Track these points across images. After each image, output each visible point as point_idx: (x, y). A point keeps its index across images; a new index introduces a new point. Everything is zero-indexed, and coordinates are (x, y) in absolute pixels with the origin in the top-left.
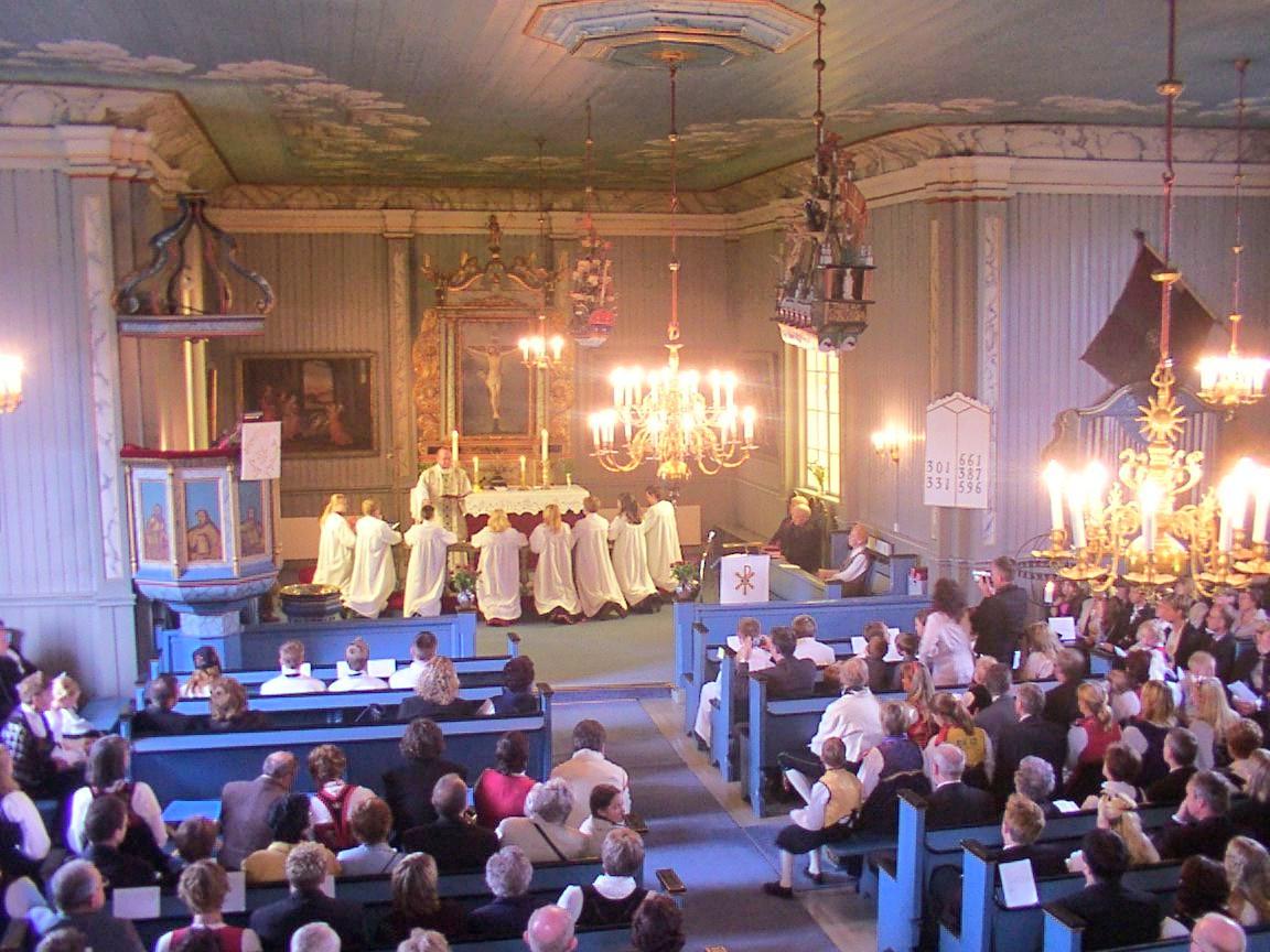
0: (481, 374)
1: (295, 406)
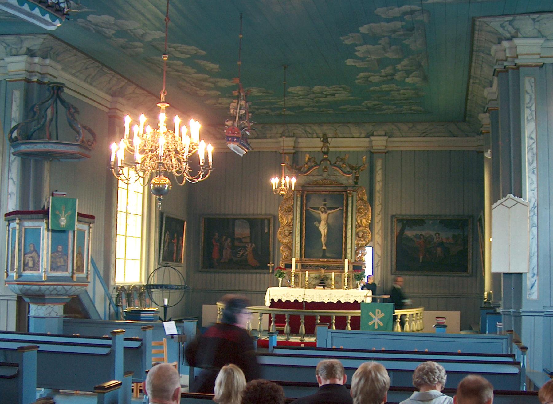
0: (316, 223)
1: (229, 244)
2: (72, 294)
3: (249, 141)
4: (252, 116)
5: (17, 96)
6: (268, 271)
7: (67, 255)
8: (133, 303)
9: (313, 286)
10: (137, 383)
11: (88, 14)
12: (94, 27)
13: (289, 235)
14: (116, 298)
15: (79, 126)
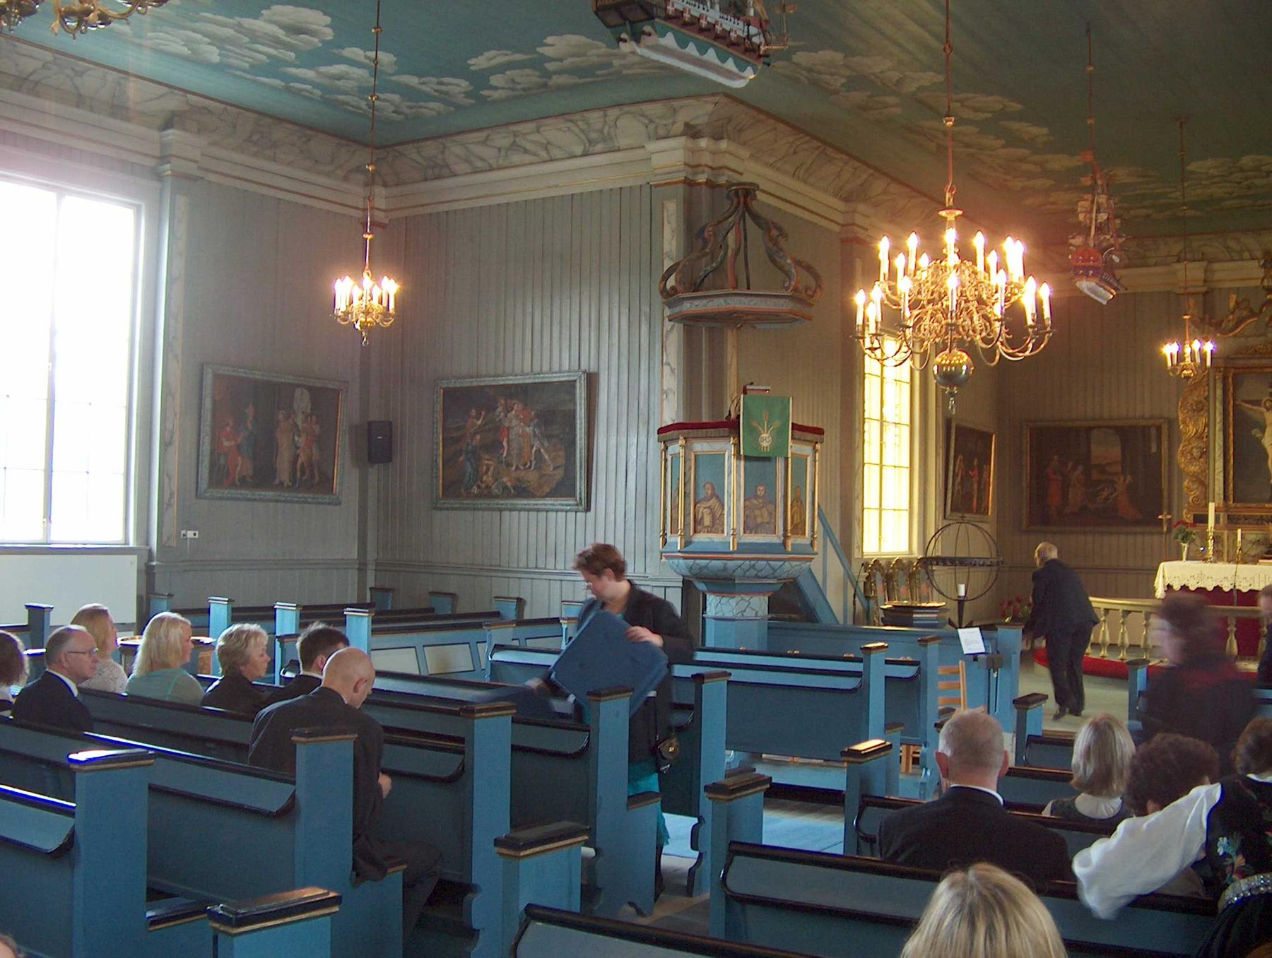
0: (1256, 432)
2: (784, 576)
3: (1119, 273)
4: (1121, 223)
5: (672, 213)
6: (1159, 529)
7: (774, 503)
8: (896, 592)
9: (1251, 558)
10: (908, 745)
11: (794, 50)
12: (805, 73)
13: (1201, 457)
14: (865, 583)
15: (789, 261)
